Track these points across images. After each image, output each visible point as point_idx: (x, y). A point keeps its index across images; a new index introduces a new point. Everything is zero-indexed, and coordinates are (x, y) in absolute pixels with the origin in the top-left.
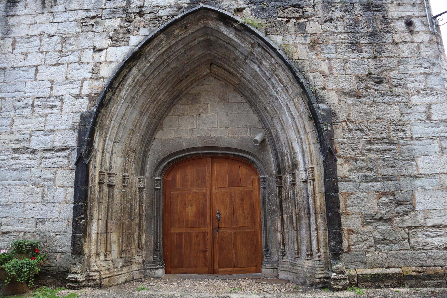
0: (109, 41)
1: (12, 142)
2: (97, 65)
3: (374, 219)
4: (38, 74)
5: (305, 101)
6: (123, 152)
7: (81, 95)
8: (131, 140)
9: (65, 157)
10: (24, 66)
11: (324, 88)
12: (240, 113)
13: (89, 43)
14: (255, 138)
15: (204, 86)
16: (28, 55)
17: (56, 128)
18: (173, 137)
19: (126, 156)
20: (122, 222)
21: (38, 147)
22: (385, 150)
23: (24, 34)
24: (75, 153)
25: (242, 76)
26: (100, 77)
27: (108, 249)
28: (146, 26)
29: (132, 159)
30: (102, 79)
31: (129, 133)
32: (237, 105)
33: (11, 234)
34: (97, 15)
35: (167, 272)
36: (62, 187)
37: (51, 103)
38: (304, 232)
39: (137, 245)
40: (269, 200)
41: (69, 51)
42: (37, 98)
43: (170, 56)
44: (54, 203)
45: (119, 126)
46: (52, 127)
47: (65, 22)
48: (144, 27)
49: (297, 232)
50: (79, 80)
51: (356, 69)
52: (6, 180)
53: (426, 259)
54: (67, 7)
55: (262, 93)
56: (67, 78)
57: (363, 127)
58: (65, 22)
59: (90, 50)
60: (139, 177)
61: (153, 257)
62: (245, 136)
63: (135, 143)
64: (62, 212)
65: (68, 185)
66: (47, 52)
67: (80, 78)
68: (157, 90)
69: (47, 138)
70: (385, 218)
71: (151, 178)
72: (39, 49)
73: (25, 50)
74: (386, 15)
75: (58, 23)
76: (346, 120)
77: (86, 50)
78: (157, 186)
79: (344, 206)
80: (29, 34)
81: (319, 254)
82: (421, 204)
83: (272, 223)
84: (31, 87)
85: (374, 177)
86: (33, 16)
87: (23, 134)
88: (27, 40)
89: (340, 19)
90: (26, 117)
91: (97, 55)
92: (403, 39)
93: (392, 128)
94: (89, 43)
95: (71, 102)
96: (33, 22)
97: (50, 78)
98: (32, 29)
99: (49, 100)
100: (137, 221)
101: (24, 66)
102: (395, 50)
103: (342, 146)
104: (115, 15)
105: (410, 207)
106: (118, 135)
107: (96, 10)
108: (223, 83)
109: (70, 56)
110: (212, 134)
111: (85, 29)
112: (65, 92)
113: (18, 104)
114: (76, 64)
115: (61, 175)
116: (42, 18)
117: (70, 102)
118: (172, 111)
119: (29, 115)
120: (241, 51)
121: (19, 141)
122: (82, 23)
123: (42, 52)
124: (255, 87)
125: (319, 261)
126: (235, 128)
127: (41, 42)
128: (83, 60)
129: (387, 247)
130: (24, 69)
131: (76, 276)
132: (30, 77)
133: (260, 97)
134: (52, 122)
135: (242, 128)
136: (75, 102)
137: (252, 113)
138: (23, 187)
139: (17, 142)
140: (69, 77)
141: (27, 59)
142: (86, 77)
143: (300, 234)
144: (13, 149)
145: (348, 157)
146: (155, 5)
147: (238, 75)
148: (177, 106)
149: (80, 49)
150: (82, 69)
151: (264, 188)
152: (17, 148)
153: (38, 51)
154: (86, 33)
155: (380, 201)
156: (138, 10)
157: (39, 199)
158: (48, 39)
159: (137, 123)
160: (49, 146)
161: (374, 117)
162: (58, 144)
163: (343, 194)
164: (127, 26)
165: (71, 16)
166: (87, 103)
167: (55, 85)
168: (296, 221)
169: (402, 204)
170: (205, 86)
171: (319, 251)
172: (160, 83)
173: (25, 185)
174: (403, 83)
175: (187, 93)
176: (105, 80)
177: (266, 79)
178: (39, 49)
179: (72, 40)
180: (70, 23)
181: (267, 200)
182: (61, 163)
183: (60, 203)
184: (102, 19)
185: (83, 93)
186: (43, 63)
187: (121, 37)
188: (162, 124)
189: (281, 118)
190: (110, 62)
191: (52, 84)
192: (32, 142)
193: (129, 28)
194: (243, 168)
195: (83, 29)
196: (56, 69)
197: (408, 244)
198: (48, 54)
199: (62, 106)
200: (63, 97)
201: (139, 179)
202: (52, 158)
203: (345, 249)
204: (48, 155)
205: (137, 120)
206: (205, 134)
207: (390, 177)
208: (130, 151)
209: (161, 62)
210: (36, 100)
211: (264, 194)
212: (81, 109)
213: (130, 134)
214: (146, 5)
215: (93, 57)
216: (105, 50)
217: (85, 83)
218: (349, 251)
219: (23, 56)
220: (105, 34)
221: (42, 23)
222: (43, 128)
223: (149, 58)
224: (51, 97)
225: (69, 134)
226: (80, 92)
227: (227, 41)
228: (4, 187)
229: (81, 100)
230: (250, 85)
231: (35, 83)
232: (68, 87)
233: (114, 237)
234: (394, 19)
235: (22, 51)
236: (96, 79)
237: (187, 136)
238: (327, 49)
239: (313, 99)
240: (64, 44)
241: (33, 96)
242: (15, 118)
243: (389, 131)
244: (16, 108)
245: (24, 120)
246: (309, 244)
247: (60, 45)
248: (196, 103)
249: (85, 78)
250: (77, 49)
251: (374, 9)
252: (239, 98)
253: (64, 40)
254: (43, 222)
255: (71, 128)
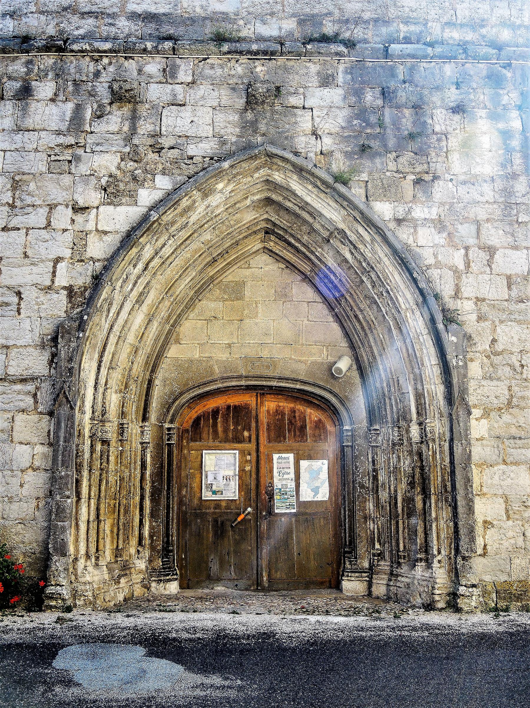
6: (120, 384)
7: (53, 287)
12: (311, 319)
15: (250, 270)
18: (197, 356)
20: (118, 502)
24: (46, 386)
25: (320, 260)
29: (131, 394)
31: (128, 350)
32: (306, 305)
34: (77, 143)
39: (137, 539)
43: (204, 225)
45: (118, 341)
48: (164, 174)
56: (26, 256)
58: (17, 150)
61: (162, 562)
62: (319, 360)
64: (26, 486)
76: (492, 356)
78: (168, 440)
79: (479, 483)
83: (360, 506)
91: (79, 218)
95: (37, 298)
100: (138, 499)
109: (31, 216)
110: (265, 354)
114: (44, 232)
115: (23, 424)
117: (34, 297)
120: (323, 223)
135: (315, 346)
136: (43, 298)
140: (29, 253)
142: (61, 256)
146: (181, 134)
150: (54, 241)
156: (150, 141)
164: (132, 168)
170: (253, 270)
175: (221, 281)
177: (362, 273)
180: (27, 153)
183: (22, 471)
184: (85, 152)
185: (57, 284)
189: (381, 336)
190: (105, 233)
193: (136, 172)
196: (5, 238)
199: (19, 304)
200: (22, 290)
201: (141, 427)
203: (480, 551)
205: (143, 329)
206: (251, 353)
209: (188, 235)
212: (56, 312)
213: (131, 352)
214: (164, 133)
215: (73, 221)
217: (59, 266)
220: (93, 181)
225: (34, 354)
226: (53, 281)
227: (299, 205)
232: (30, 271)
233: (107, 526)
249: (59, 257)
255: (39, 344)
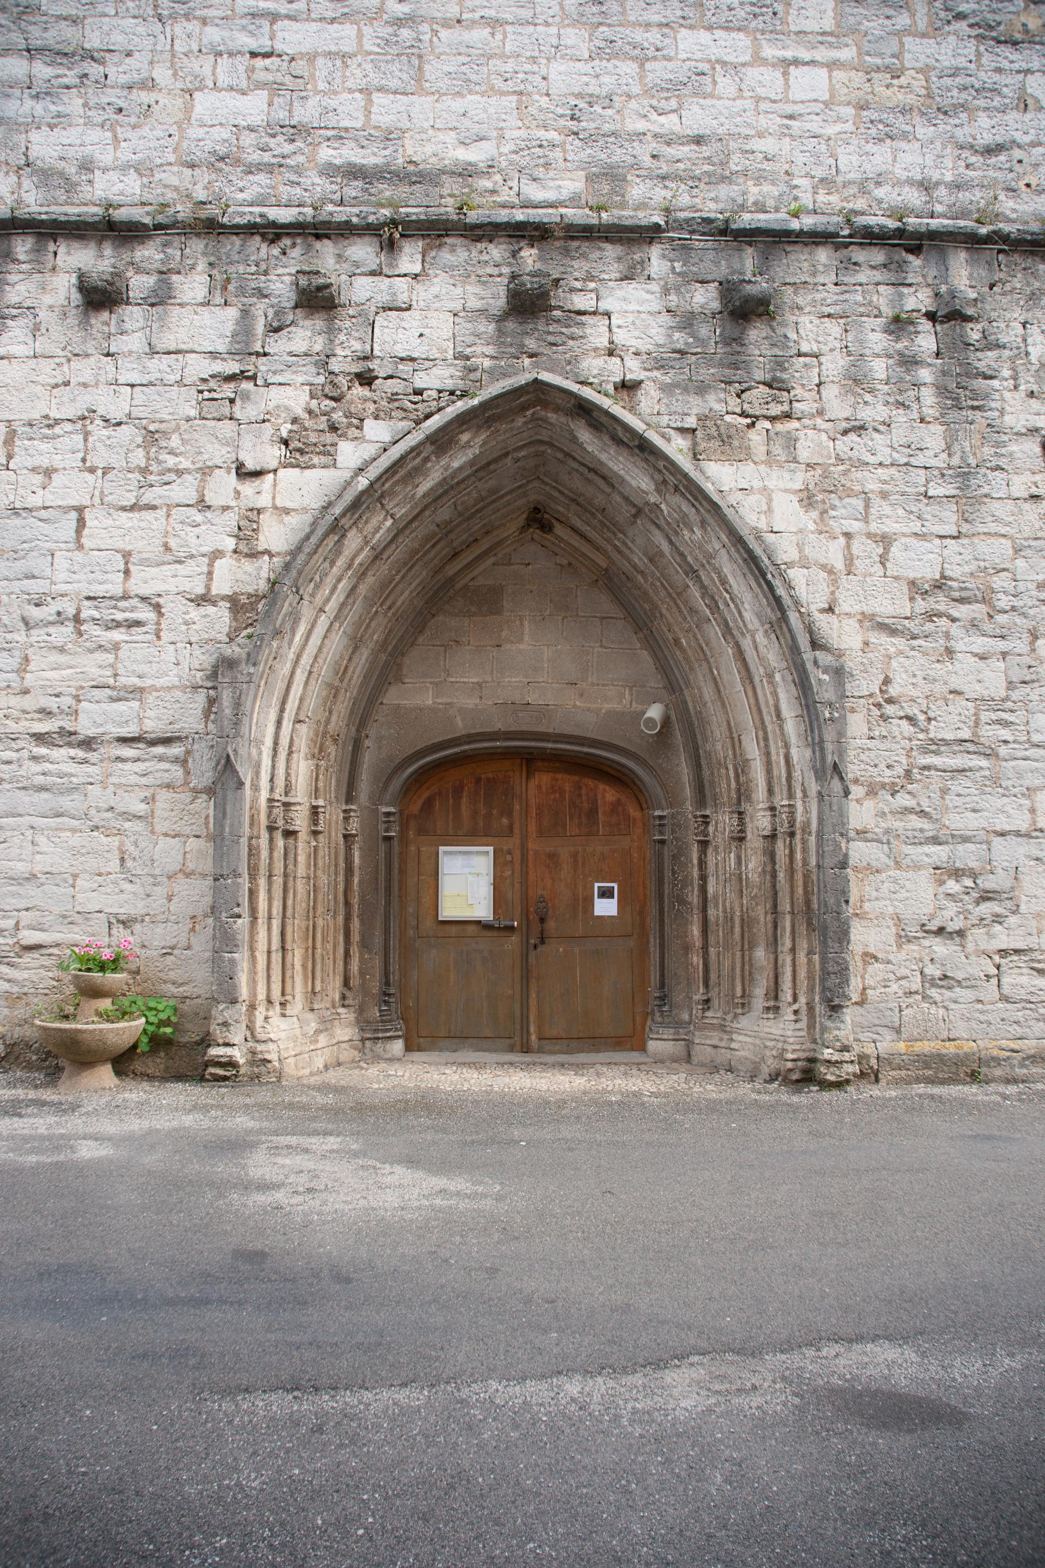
0: (279, 451)
1: (28, 716)
2: (253, 515)
3: (926, 932)
4: (86, 532)
5: (782, 641)
8: (330, 712)
9: (176, 760)
10: (45, 508)
11: (830, 610)
13: (224, 452)
14: (647, 715)
16: (54, 476)
17: (148, 682)
19: (318, 753)
21: (101, 730)
22: (964, 770)
23: (36, 415)
26: (260, 549)
27: (288, 989)
28: (382, 414)
30: (266, 558)
33: (44, 951)
34: (242, 372)
35: (408, 1048)
36: (174, 837)
37: (128, 615)
38: (760, 954)
40: (674, 873)
41: (169, 470)
42: (89, 598)
44: (154, 876)
45: (308, 679)
46: (136, 681)
47: (151, 384)
49: (743, 956)
50: (203, 555)
51: (910, 563)
52: (20, 815)
53: (1032, 1023)
54: (154, 342)
55: (671, 603)
56: (167, 548)
57: (916, 712)
58: (151, 384)
59: (229, 473)
60: (344, 807)
63: (337, 723)
64: (175, 899)
65: (187, 830)
66: (106, 471)
67: (204, 549)
68: (399, 582)
69: (121, 707)
70: (949, 929)
71: (373, 810)
72: (84, 460)
73: (45, 462)
74: (997, 422)
75: (132, 386)
77: (217, 471)
78: (387, 831)
80: (52, 415)
81: (795, 1007)
82: (1034, 900)
84: (67, 566)
85: (931, 834)
86: (57, 360)
87: (57, 696)
88: (46, 431)
89: (882, 428)
90: (62, 650)
91: (248, 488)
92: (1034, 491)
93: (985, 716)
94: (224, 452)
96: (60, 380)
97: (120, 545)
98: (57, 400)
99: (122, 604)
101: (45, 508)
102: (1011, 519)
103: (863, 757)
104: (294, 377)
105: (1009, 904)
106: (306, 704)
107: (237, 357)
108: (565, 562)
109: (174, 486)
111: (211, 409)
112: (166, 587)
113: (35, 613)
114: (192, 511)
116: (83, 370)
118: (428, 632)
119: (70, 646)
121: (46, 713)
122: (201, 392)
123: (92, 470)
124: (652, 584)
125: (796, 1021)
126: (593, 684)
127: (86, 440)
128: (210, 499)
129: (947, 994)
130: (43, 514)
131: (228, 1051)
132: (63, 539)
133: (664, 611)
134: (135, 666)
137: (638, 645)
138: (69, 834)
139: (40, 716)
140: (173, 543)
141: (50, 488)
143: (750, 959)
144: (34, 735)
145: (876, 783)
147: (609, 548)
148: (440, 618)
149: (200, 469)
151: (662, 842)
152: (43, 731)
153: (81, 464)
154: (213, 423)
155: (941, 889)
156: (356, 368)
157: (114, 865)
158: (105, 432)
159: (346, 667)
160: (131, 730)
161: (945, 689)
162: (153, 725)
163: (856, 869)
165: (168, 370)
166: (227, 620)
167: (134, 564)
168: (742, 927)
169: (989, 899)
170: (516, 567)
171: (795, 999)
172: (405, 564)
173: (74, 830)
174: (1021, 603)
176: (275, 559)
178: (84, 460)
179: (175, 441)
180: (167, 388)
181: (668, 874)
182: (166, 775)
183: (169, 878)
186: (97, 500)
187: (314, 441)
188: (400, 666)
190: (287, 511)
191: (126, 563)
192: (82, 716)
194: (607, 788)
195: (205, 409)
197: (996, 988)
198: (108, 477)
200: (161, 600)
201: (345, 811)
202: (138, 760)
203: (855, 997)
204: (127, 752)
207: (970, 833)
208: (329, 742)
210: (86, 603)
211: (660, 857)
213: (328, 697)
214: (376, 353)
215: (238, 493)
216: (271, 475)
217: (218, 563)
218: (861, 1003)
219: (38, 479)
221: (85, 385)
222: (111, 681)
223: (391, 505)
224: (125, 597)
226: (208, 588)
228: (16, 833)
229: (211, 610)
230: (639, 577)
231: (78, 556)
234: (1016, 434)
235: (37, 463)
236: (247, 555)
237: (470, 702)
238: (844, 507)
239: (803, 642)
240: (154, 450)
241: (78, 594)
242: (30, 652)
243: (977, 723)
244: (32, 623)
245: (55, 657)
246: (772, 984)
247: (140, 453)
248: (492, 613)
250: (192, 467)
251: (970, 403)
252: (605, 604)
253: (152, 438)
254: (126, 923)
